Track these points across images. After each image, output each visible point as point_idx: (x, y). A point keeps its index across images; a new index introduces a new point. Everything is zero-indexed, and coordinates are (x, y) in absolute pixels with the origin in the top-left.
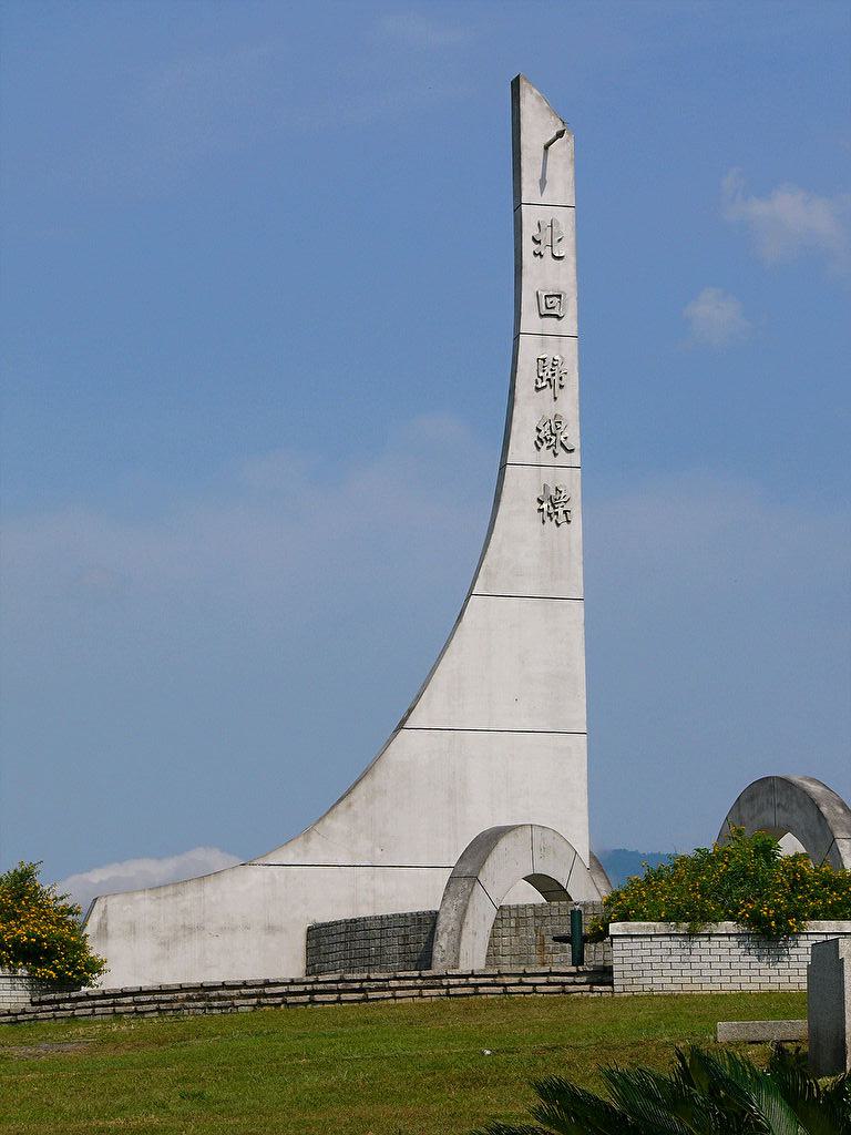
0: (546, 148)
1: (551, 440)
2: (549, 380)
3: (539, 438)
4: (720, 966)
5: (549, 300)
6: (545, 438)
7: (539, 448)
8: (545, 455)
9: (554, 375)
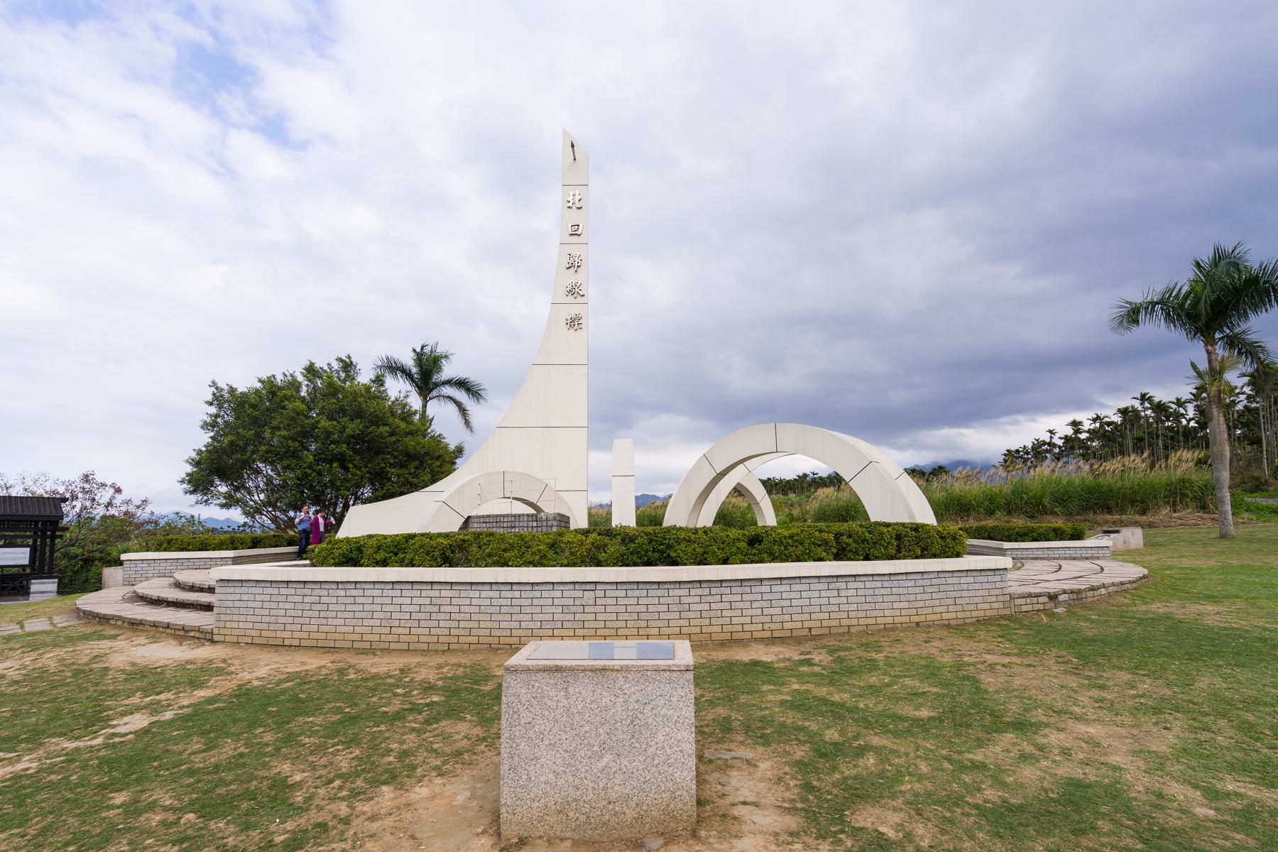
4: (293, 613)
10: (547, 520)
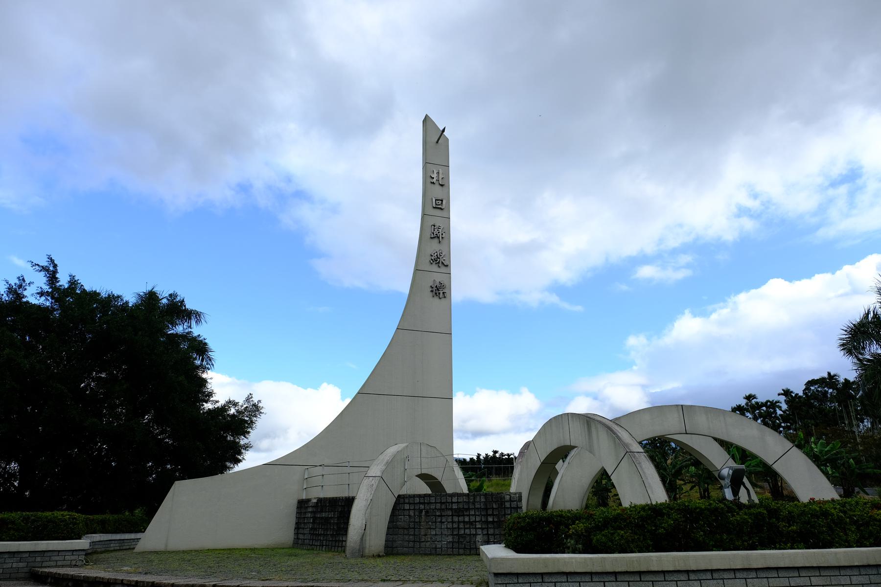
0: (437, 142)
1: (437, 260)
2: (437, 234)
3: (432, 260)
5: (437, 202)
6: (435, 259)
7: (432, 264)
8: (434, 267)
9: (439, 233)
10: (511, 501)
